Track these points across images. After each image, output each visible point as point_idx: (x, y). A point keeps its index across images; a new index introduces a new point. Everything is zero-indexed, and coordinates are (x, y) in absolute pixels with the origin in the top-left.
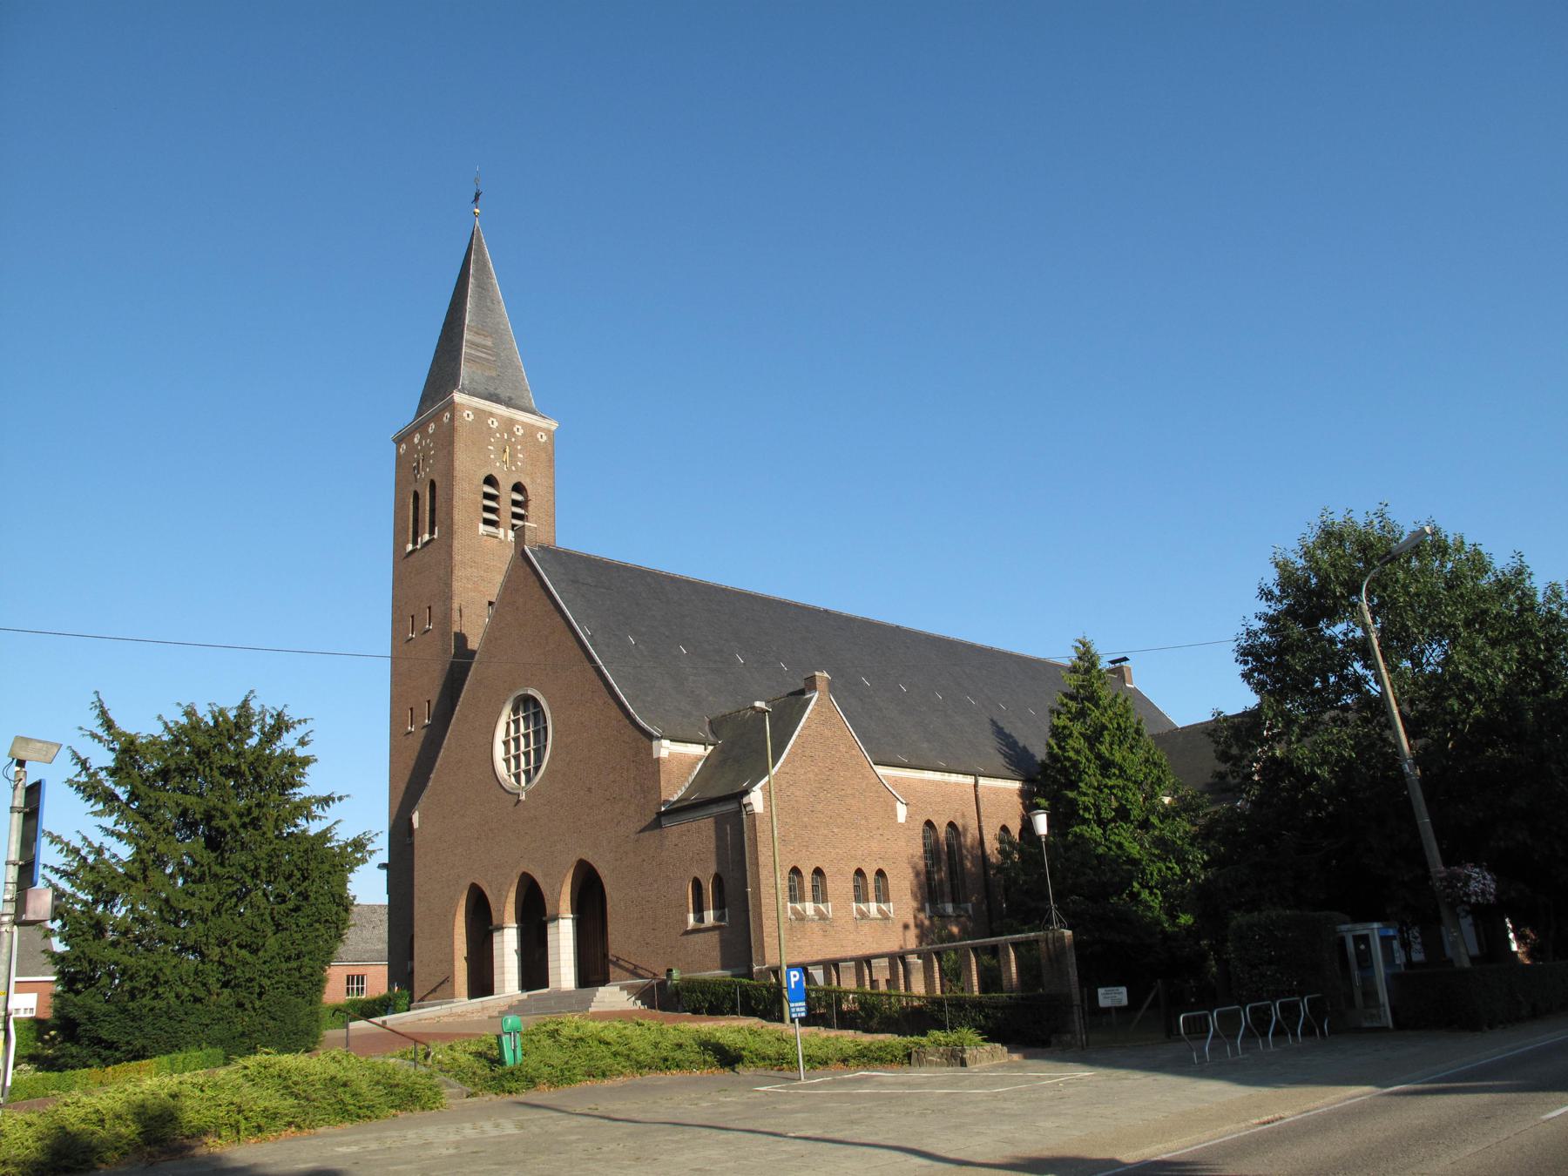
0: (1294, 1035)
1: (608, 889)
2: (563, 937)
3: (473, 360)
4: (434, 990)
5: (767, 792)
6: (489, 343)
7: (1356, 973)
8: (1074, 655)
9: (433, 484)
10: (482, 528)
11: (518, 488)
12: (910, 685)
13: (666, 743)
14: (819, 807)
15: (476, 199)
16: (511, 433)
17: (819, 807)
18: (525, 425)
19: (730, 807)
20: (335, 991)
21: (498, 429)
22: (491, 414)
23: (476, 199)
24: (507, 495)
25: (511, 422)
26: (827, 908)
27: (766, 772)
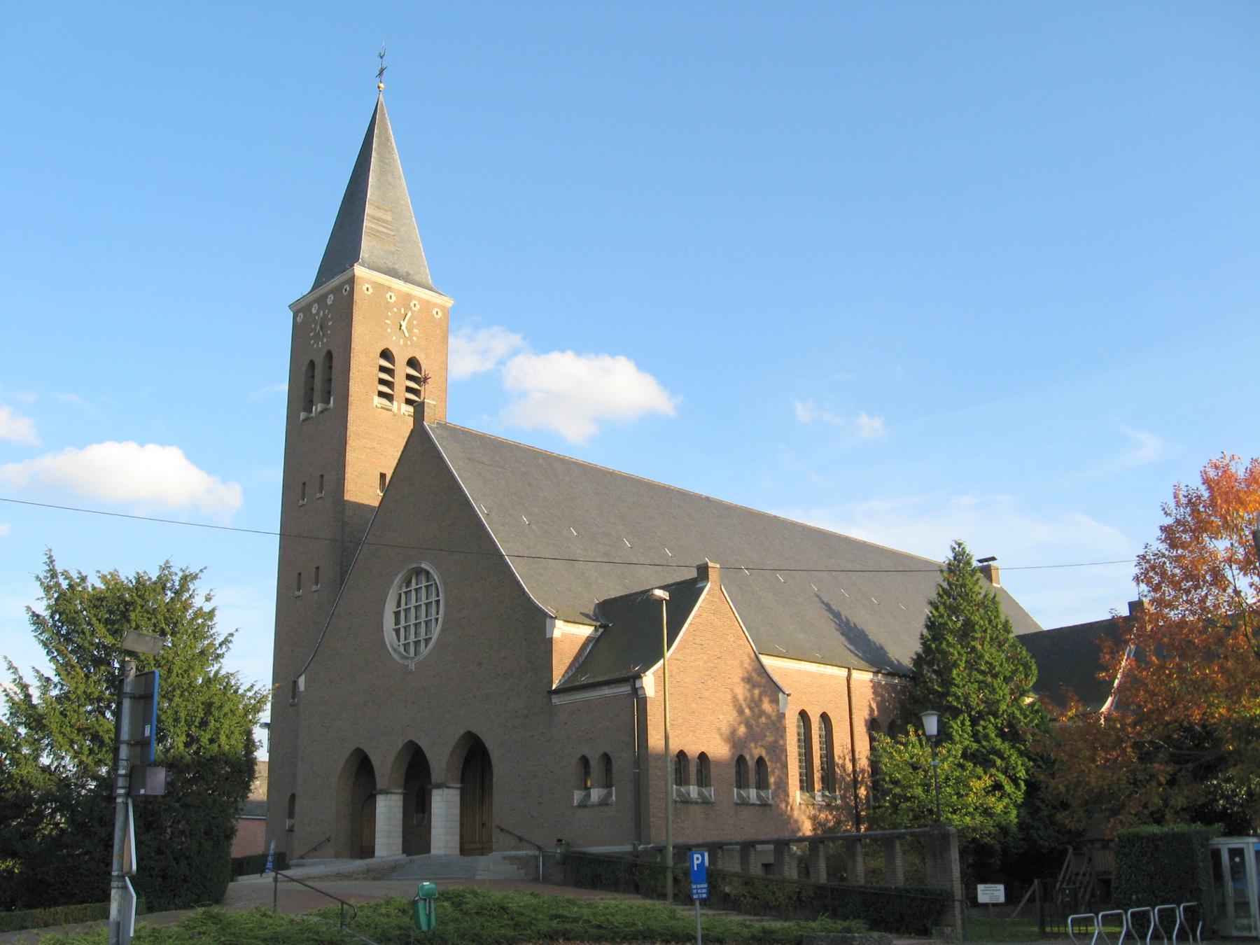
0: (1170, 939)
1: (495, 762)
2: (444, 806)
3: (375, 234)
4: (315, 849)
5: (662, 680)
6: (389, 218)
7: (1230, 885)
8: (951, 556)
9: (329, 355)
10: (378, 401)
11: (413, 363)
12: (807, 575)
13: (559, 623)
14: (707, 694)
15: (381, 73)
16: (408, 308)
17: (707, 694)
18: (421, 301)
19: (625, 689)
20: (239, 848)
21: (391, 306)
22: (389, 289)
23: (381, 73)
24: (402, 369)
25: (408, 298)
26: (711, 792)
27: (661, 656)
